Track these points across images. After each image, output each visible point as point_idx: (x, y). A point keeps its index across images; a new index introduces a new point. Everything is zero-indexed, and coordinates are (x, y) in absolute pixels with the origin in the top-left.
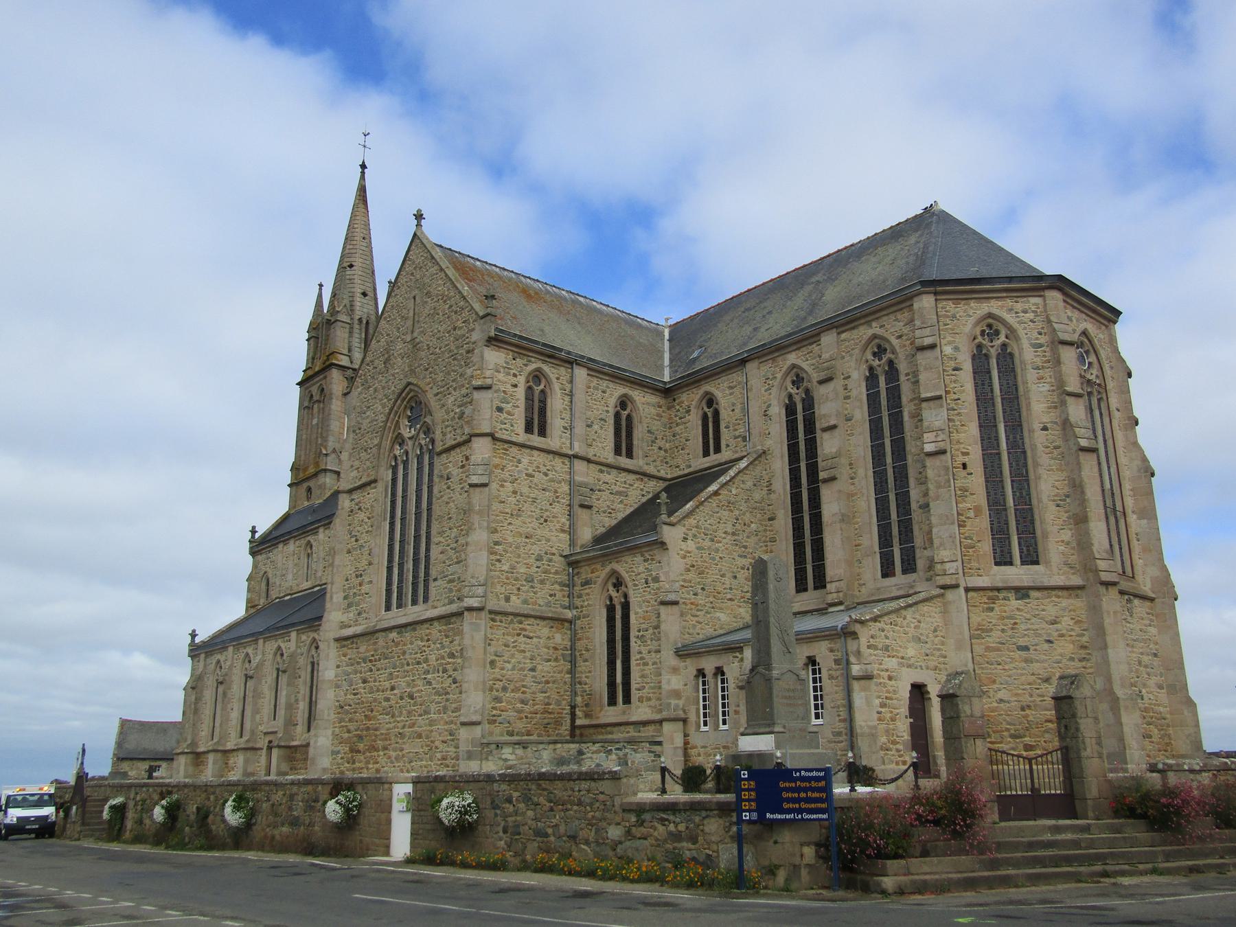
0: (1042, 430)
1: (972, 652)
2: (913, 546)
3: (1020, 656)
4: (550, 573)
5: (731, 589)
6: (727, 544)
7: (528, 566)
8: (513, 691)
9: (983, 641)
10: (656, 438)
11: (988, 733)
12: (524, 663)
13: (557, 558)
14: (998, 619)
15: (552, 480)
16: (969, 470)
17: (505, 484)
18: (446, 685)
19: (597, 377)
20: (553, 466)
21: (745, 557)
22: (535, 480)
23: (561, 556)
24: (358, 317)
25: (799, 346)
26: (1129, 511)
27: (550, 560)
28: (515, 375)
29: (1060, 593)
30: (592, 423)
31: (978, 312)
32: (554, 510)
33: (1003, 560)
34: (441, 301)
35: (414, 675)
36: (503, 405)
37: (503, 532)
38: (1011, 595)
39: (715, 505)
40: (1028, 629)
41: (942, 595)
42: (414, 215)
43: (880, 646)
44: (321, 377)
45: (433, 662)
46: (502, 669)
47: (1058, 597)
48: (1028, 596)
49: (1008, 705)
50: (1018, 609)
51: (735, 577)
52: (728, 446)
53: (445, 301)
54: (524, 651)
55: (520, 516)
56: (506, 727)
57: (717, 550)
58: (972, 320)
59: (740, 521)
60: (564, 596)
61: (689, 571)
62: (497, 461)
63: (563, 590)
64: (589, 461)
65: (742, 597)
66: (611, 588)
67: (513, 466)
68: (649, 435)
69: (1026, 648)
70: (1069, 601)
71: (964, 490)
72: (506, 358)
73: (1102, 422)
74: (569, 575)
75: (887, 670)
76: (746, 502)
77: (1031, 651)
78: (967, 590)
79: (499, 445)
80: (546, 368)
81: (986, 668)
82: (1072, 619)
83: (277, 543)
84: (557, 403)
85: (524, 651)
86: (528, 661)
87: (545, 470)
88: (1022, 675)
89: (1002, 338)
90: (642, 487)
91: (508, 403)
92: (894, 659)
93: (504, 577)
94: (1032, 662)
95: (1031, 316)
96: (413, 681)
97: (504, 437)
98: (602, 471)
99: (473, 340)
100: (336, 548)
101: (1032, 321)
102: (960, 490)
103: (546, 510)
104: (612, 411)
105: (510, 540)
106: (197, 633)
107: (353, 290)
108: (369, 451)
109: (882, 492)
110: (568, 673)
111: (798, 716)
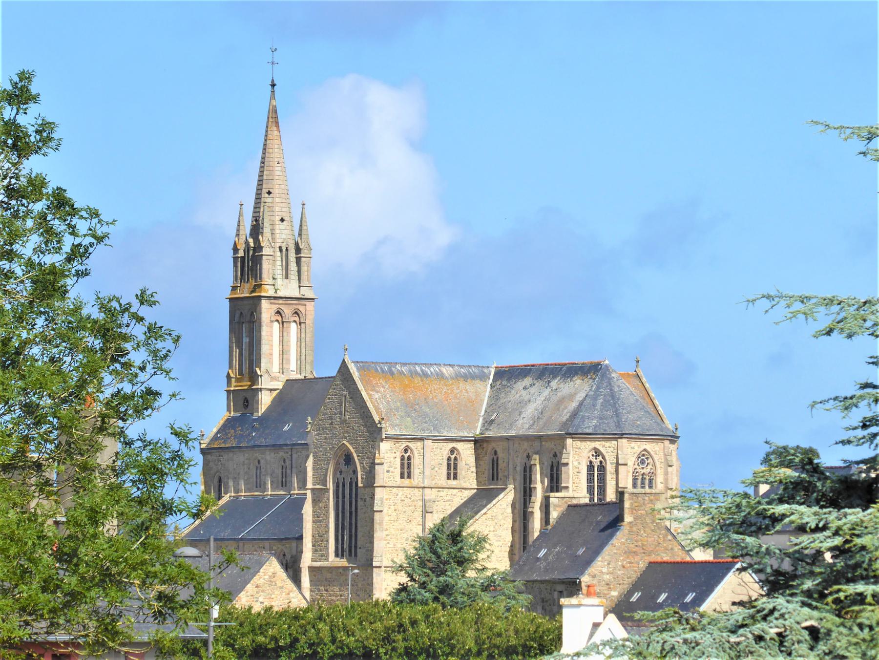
15: (413, 501)
22: (405, 502)
24: (278, 245)
45: (360, 585)
58: (587, 450)
84: (416, 461)
95: (612, 449)
98: (439, 491)
105: (393, 533)
107: (272, 218)
109: (590, 483)
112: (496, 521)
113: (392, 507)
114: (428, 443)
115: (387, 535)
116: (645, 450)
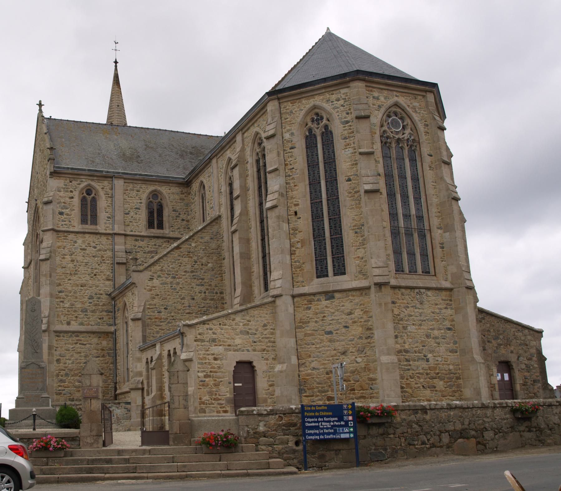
0: (347, 181)
1: (296, 338)
3: (327, 338)
4: (99, 306)
5: (190, 306)
6: (186, 278)
7: (83, 303)
8: (73, 376)
9: (303, 330)
10: (180, 214)
11: (304, 390)
12: (80, 359)
13: (104, 296)
14: (313, 314)
15: (100, 250)
16: (298, 216)
17: (66, 257)
19: (132, 183)
20: (100, 242)
21: (202, 285)
22: (87, 252)
23: (107, 295)
25: (229, 145)
27: (99, 298)
28: (71, 192)
29: (354, 293)
31: (307, 106)
32: (102, 268)
33: (322, 273)
36: (63, 211)
37: (65, 285)
38: (322, 298)
39: (176, 255)
40: (333, 320)
41: (274, 302)
46: (65, 363)
47: (353, 296)
48: (333, 297)
49: (318, 371)
50: (326, 306)
51: (193, 299)
54: (80, 353)
55: (77, 274)
56: (69, 396)
57: (178, 284)
59: (198, 263)
60: (109, 318)
61: (154, 298)
62: (59, 244)
63: (108, 315)
67: (71, 245)
68: (174, 213)
69: (330, 333)
70: (361, 298)
71: (295, 229)
72: (65, 182)
75: (213, 354)
76: (203, 250)
77: (334, 335)
78: (293, 297)
79: (61, 234)
80: (93, 183)
81: (305, 348)
82: (362, 310)
84: (103, 203)
85: (80, 353)
86: (83, 358)
87: (94, 245)
88: (327, 350)
89: (325, 121)
91: (67, 209)
92: (220, 347)
93: (66, 311)
94: (334, 342)
95: (342, 102)
97: (64, 229)
98: (136, 240)
101: (342, 106)
102: (293, 230)
103: (96, 269)
105: (70, 289)
110: (112, 363)
111: (38, 389)
112: (195, 258)
113: (68, 258)
114: (119, 184)
115: (60, 292)
116: (396, 105)
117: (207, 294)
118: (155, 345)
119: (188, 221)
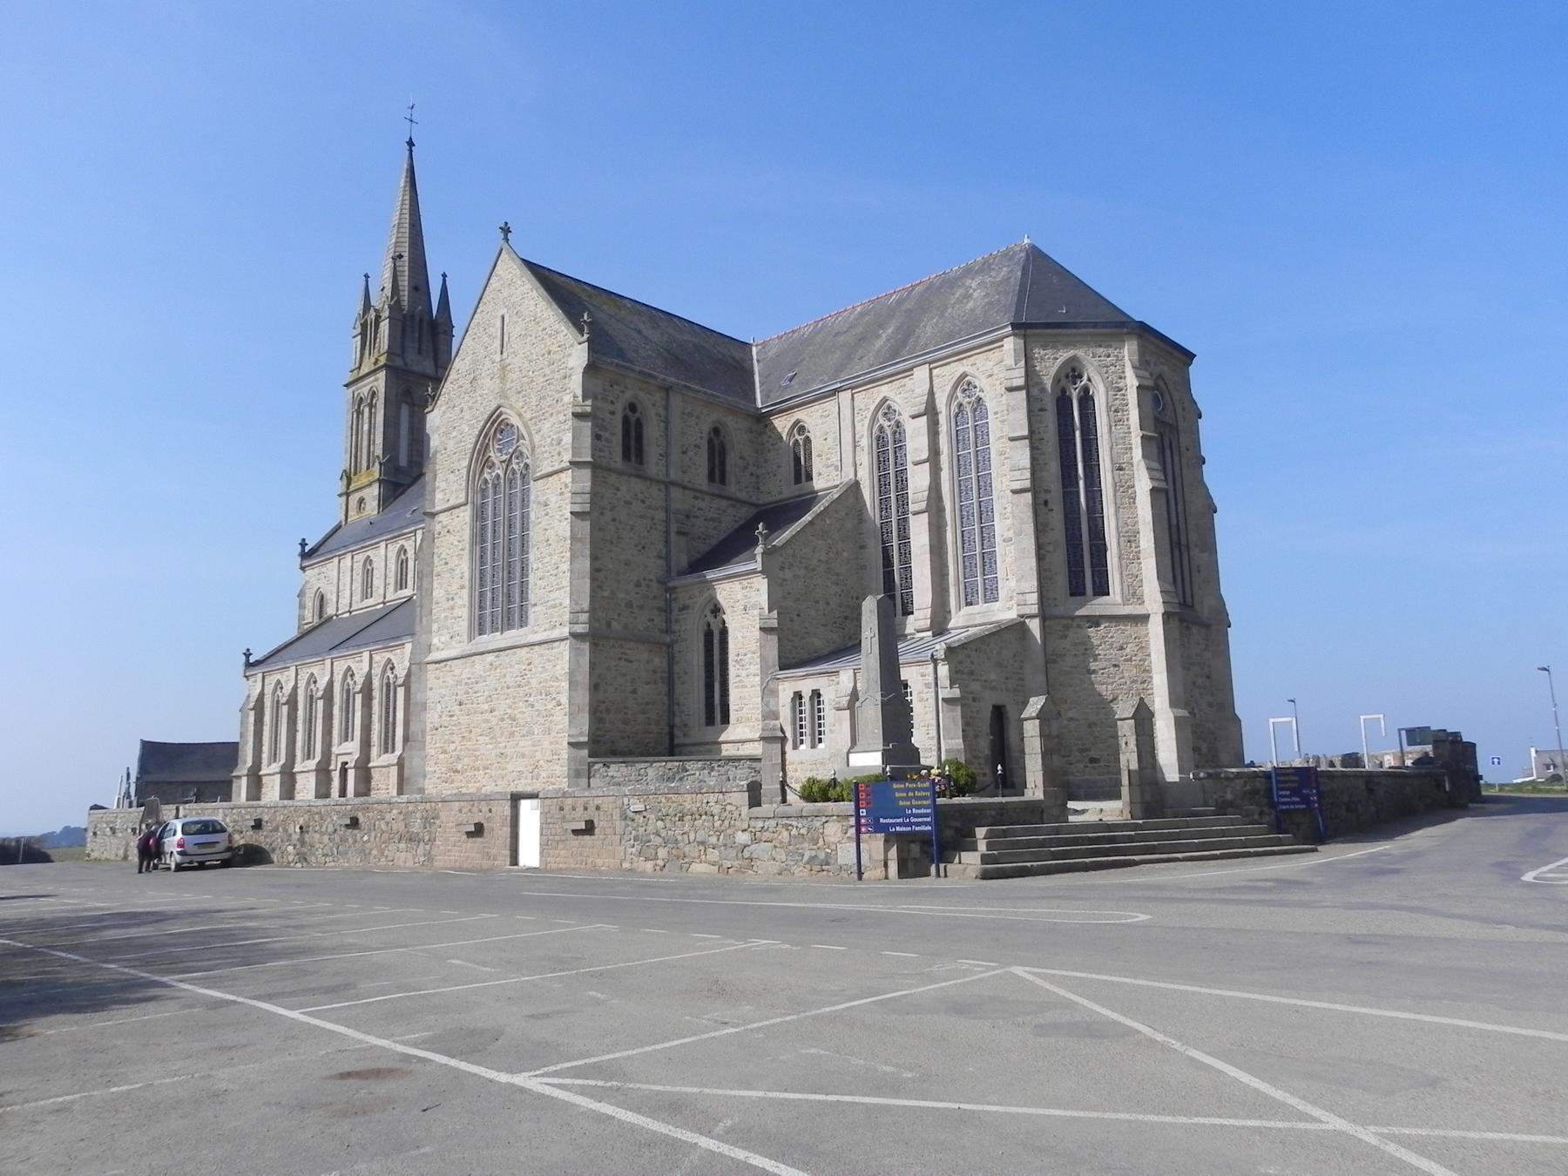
2: (996, 577)
10: (748, 464)
13: (655, 585)
15: (649, 507)
18: (550, 706)
26: (1191, 546)
28: (612, 402)
30: (687, 449)
34: (533, 323)
35: (515, 697)
42: (501, 228)
43: (966, 671)
44: (372, 378)
51: (828, 604)
52: (820, 474)
53: (538, 323)
64: (684, 488)
65: (835, 623)
66: (708, 614)
73: (1172, 461)
74: (666, 600)
75: (971, 693)
83: (332, 558)
84: (652, 431)
85: (624, 675)
90: (734, 512)
96: (514, 703)
98: (696, 498)
99: (570, 366)
100: (424, 571)
104: (705, 436)
106: (251, 652)
108: (457, 473)
117: (842, 597)
118: (838, 672)
119: (757, 477)
